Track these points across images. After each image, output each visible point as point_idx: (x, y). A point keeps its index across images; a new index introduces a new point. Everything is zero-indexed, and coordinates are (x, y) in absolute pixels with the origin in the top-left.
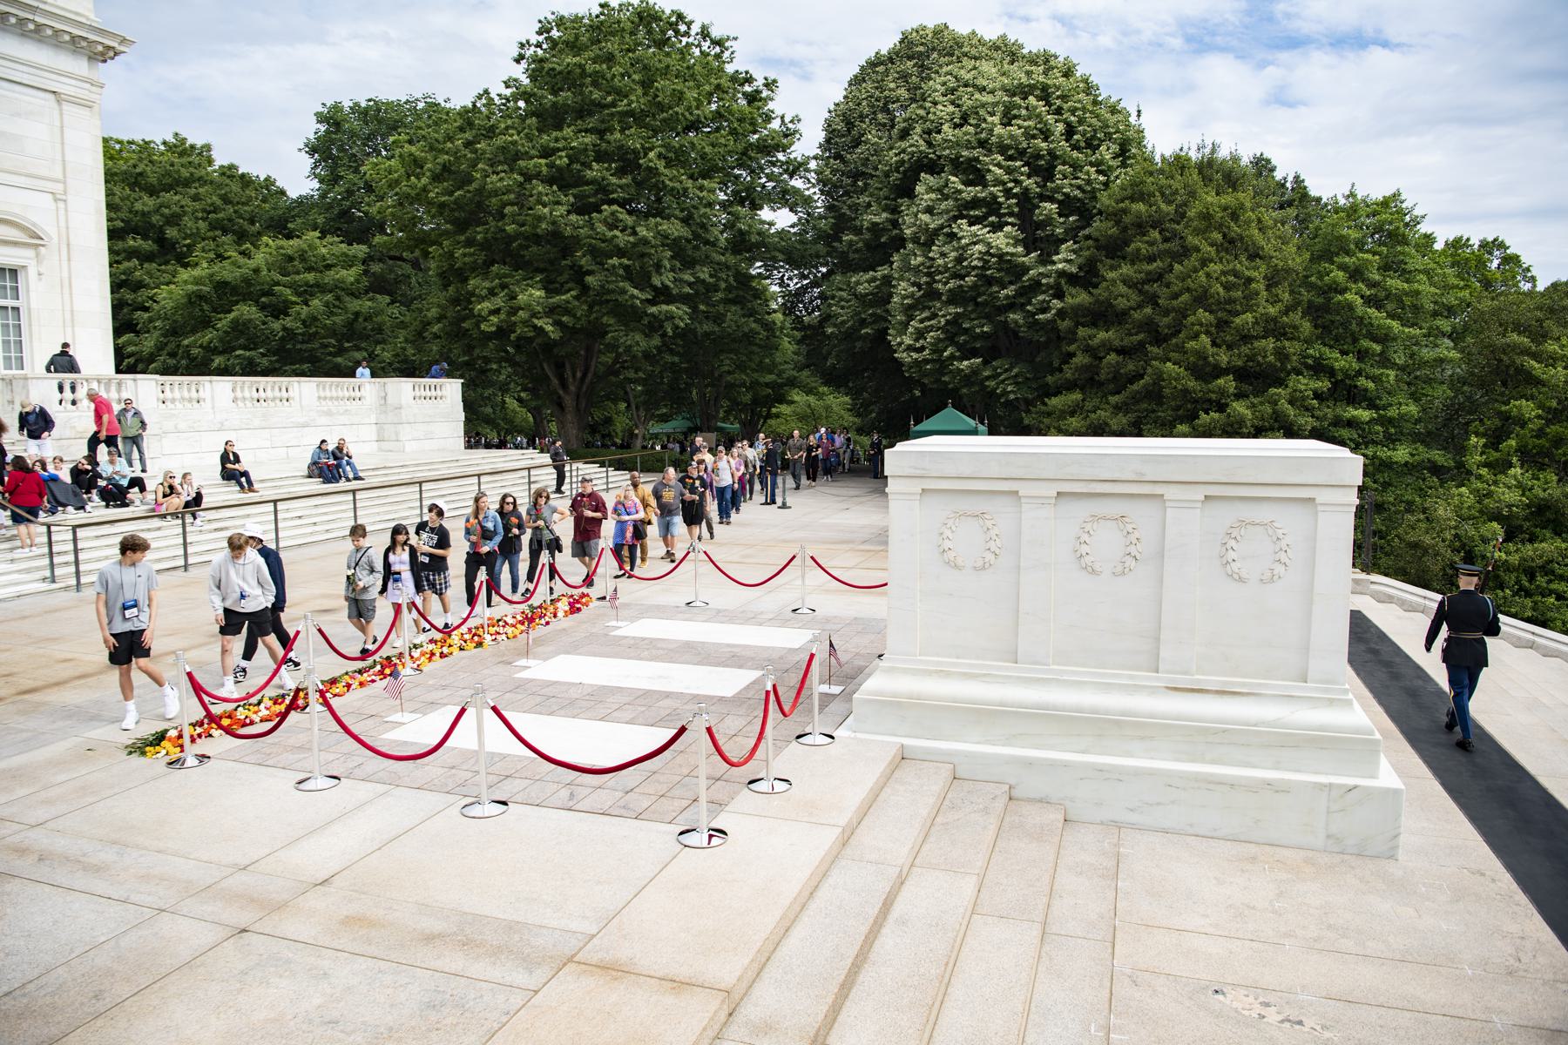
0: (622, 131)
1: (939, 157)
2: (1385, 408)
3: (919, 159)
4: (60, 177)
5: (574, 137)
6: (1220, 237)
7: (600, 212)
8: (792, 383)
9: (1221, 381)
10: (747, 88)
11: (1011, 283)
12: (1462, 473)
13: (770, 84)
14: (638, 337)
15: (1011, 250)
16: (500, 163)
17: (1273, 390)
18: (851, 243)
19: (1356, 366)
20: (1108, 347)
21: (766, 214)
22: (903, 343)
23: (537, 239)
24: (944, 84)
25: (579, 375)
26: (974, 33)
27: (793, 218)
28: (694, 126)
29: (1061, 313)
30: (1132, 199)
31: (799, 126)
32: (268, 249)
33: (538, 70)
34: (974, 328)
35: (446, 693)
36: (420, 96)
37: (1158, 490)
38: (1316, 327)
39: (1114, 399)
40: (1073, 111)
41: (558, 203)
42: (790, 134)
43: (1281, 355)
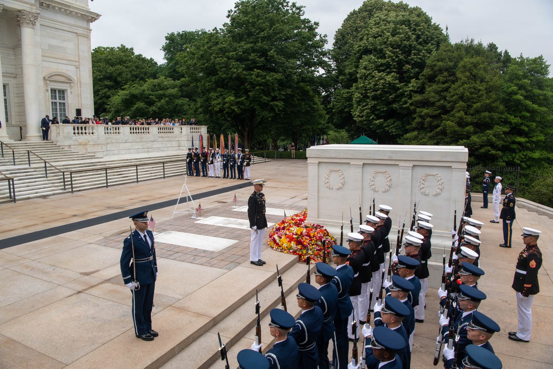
2: (531, 137)
9: (468, 128)
13: (317, 24)
15: (394, 82)
17: (488, 131)
18: (342, 79)
19: (520, 121)
20: (428, 115)
24: (375, 21)
30: (438, 61)
32: (146, 86)
37: (397, 163)
38: (506, 107)
39: (429, 134)
40: (420, 30)
42: (323, 41)
43: (492, 119)
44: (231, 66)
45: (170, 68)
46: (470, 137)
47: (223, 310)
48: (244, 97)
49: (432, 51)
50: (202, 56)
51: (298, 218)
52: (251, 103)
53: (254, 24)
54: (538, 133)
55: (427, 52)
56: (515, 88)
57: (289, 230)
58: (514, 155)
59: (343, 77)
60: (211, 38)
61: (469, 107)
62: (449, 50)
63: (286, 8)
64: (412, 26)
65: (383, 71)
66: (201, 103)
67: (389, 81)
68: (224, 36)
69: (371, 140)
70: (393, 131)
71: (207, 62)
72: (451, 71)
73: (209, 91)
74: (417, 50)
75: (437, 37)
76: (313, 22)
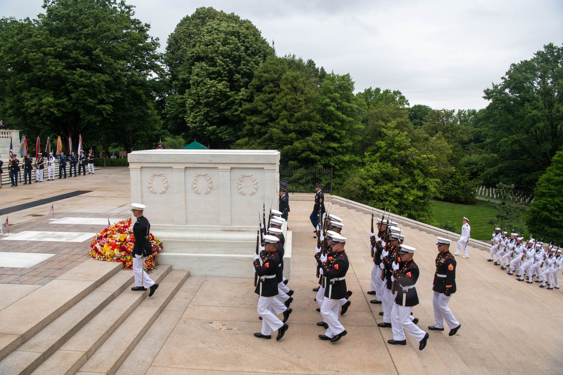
0: (85, 41)
2: (342, 143)
5: (65, 41)
6: (290, 86)
9: (291, 135)
12: (363, 164)
13: (148, 26)
15: (225, 90)
17: (308, 138)
18: (176, 85)
19: (333, 129)
20: (256, 123)
22: (189, 119)
24: (207, 29)
28: (115, 38)
29: (242, 112)
30: (264, 72)
37: (216, 166)
38: (322, 116)
39: (258, 141)
40: (248, 42)
42: (155, 44)
43: (311, 127)
44: (48, 63)
46: (293, 143)
47: (33, 325)
48: (66, 99)
49: (259, 63)
50: (10, 49)
51: (123, 225)
52: (74, 105)
53: (75, 19)
54: (347, 140)
55: (255, 64)
56: (328, 100)
57: (111, 237)
58: (329, 158)
59: (177, 83)
60: (22, 29)
61: (292, 116)
62: (274, 64)
63: (113, 6)
64: (241, 37)
65: (215, 79)
66: (10, 103)
67: (220, 89)
68: (40, 28)
69: (202, 146)
70: (226, 137)
71: (17, 56)
72: (275, 82)
73: (20, 90)
74: (246, 61)
75: (264, 50)
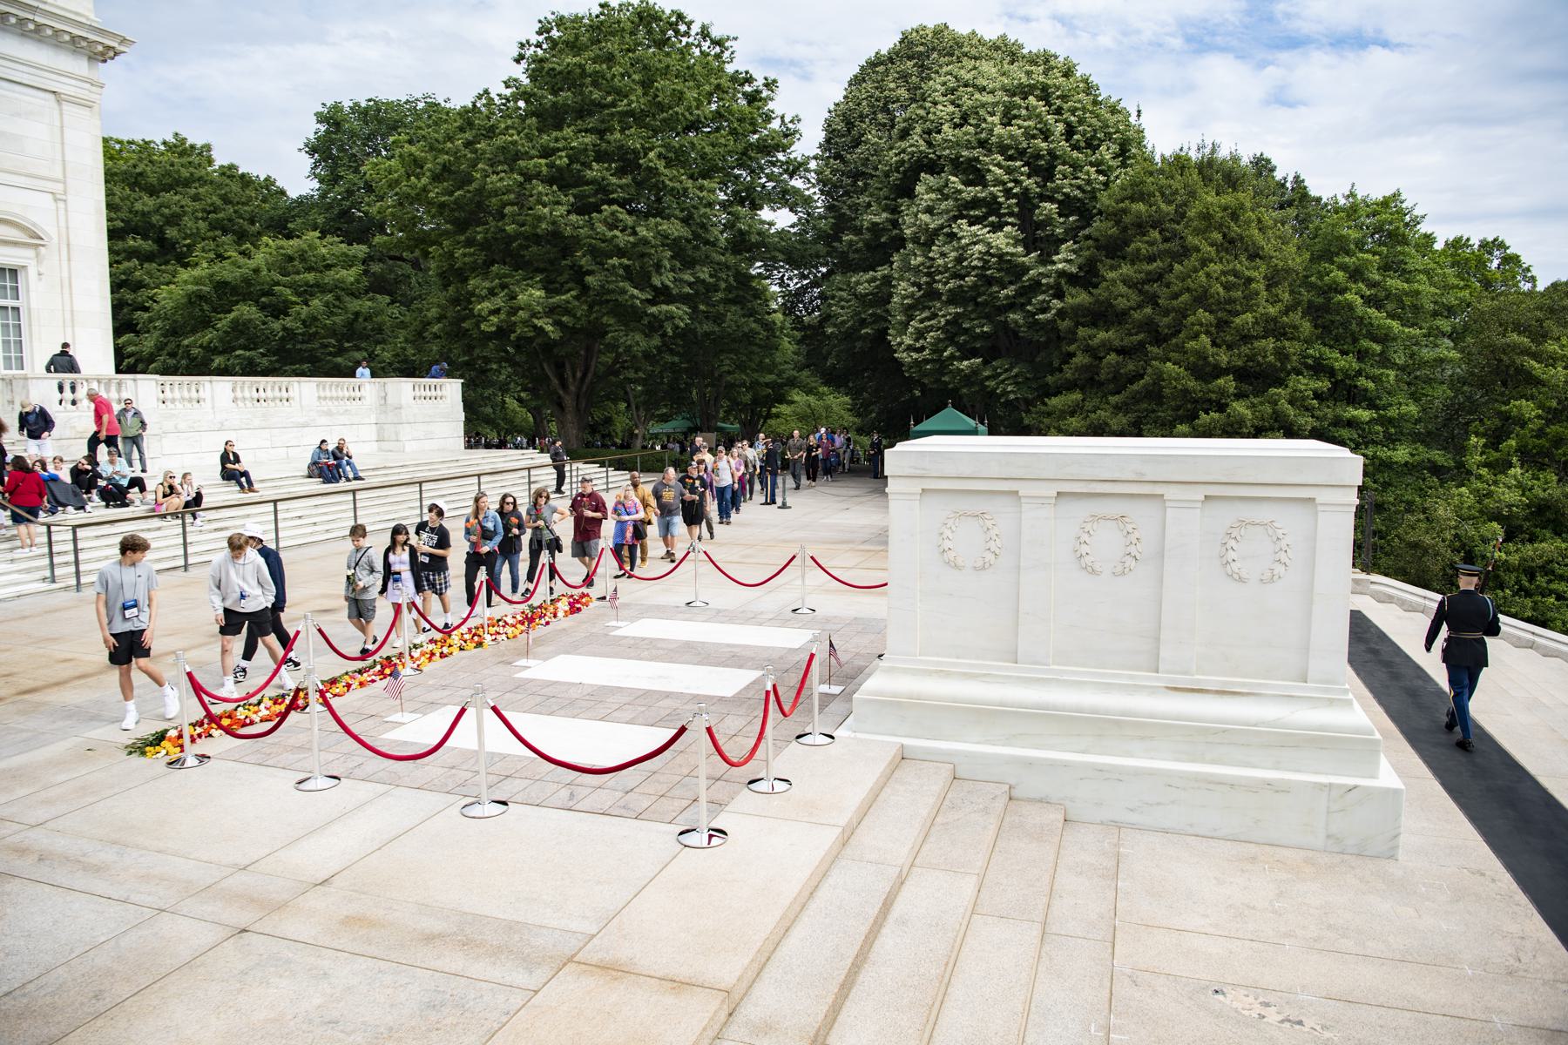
0: (622, 131)
1: (939, 157)
2: (1385, 408)
3: (919, 159)
4: (60, 177)
5: (574, 137)
6: (1220, 237)
7: (600, 212)
8: (792, 383)
9: (1221, 381)
10: (747, 88)
11: (1011, 283)
12: (1462, 473)
13: (770, 84)
14: (638, 337)
15: (1011, 250)
16: (500, 163)
17: (1273, 390)
18: (851, 243)
19: (1356, 366)
20: (1108, 347)
21: (766, 214)
22: (903, 343)
23: (537, 239)
24: (944, 84)
25: (579, 375)
26: (974, 33)
27: (793, 218)
28: (694, 126)
29: (1061, 313)
30: (1132, 199)
31: (799, 126)
32: (268, 249)
33: (538, 70)
34: (974, 328)
35: (446, 693)
36: (420, 96)
37: (1158, 490)
39: (1114, 399)
40: (1073, 111)
41: (558, 203)
42: (790, 134)
43: (1281, 355)
45: (330, 207)
76: (760, 83)
